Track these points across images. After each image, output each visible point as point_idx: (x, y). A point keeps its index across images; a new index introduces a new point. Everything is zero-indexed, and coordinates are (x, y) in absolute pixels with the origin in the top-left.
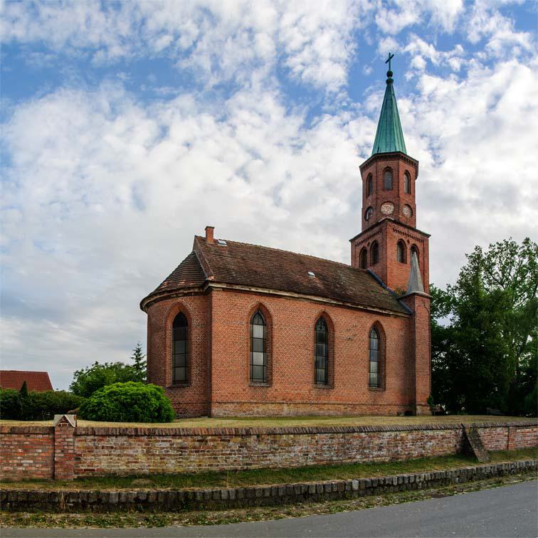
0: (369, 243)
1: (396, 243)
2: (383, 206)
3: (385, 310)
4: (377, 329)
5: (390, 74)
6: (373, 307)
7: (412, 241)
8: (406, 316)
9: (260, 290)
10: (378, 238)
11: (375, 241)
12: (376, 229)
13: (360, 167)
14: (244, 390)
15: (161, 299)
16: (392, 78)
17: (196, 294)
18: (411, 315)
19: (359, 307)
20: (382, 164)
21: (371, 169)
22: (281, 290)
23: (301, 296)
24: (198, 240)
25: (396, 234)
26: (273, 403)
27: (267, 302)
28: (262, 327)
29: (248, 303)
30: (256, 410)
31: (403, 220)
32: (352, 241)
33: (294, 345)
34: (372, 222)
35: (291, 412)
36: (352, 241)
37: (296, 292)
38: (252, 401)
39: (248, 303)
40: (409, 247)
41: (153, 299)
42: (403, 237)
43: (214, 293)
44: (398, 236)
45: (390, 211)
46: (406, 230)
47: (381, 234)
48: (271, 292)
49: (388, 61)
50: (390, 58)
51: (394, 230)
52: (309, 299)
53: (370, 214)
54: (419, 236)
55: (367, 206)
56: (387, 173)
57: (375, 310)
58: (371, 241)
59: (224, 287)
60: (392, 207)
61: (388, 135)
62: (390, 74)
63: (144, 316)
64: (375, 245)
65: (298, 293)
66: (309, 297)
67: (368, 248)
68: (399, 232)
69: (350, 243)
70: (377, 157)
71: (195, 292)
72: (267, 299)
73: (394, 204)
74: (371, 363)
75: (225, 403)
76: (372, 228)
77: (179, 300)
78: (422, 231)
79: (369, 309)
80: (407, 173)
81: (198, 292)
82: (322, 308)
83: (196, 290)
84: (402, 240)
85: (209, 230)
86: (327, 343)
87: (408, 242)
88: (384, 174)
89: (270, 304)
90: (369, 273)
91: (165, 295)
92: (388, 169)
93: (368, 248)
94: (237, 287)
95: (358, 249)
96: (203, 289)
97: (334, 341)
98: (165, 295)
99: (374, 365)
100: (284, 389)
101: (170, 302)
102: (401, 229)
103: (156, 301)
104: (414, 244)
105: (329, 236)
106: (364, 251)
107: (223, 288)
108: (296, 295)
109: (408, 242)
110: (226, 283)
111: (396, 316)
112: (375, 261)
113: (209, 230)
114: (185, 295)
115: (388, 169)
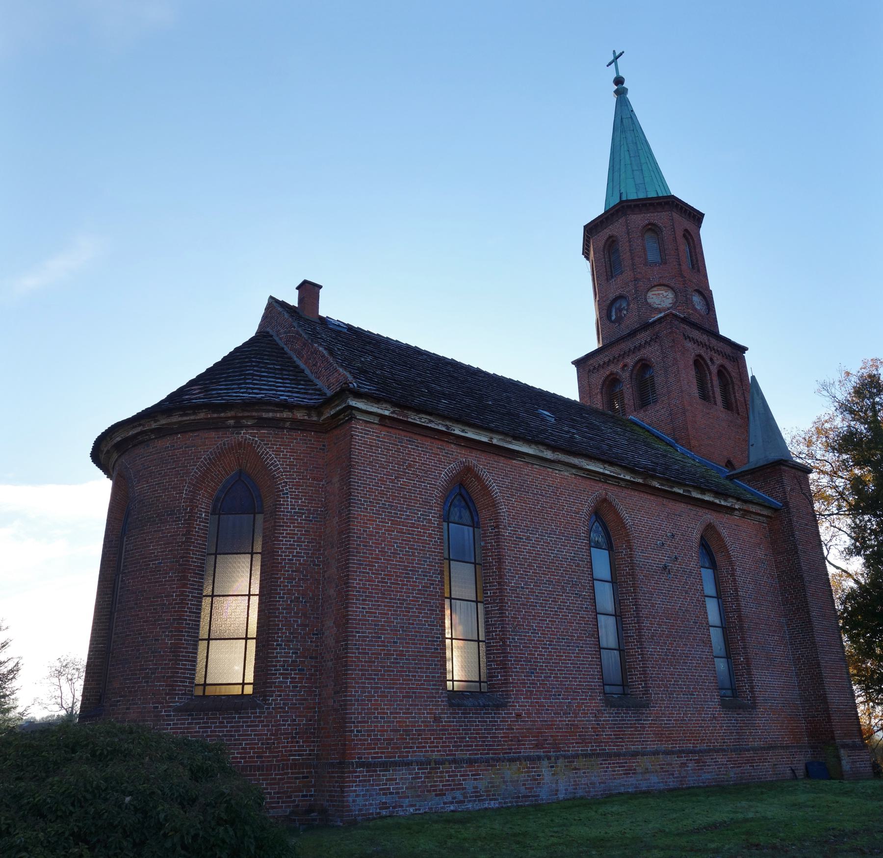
0: (625, 366)
1: (691, 362)
2: (650, 294)
3: (725, 495)
5: (619, 81)
8: (765, 512)
9: (471, 435)
10: (652, 353)
13: (585, 227)
15: (184, 429)
17: (298, 426)
19: (676, 490)
20: (638, 220)
21: (616, 229)
25: (689, 345)
27: (480, 463)
28: (471, 529)
29: (439, 465)
30: (469, 785)
31: (695, 319)
32: (578, 363)
33: (550, 582)
34: (631, 321)
35: (562, 787)
36: (578, 363)
37: (549, 447)
38: (459, 755)
39: (439, 465)
40: (714, 369)
41: (154, 425)
42: (702, 351)
43: (358, 429)
44: (693, 350)
46: (704, 338)
47: (656, 347)
48: (495, 441)
50: (617, 58)
51: (686, 337)
52: (574, 466)
54: (728, 350)
55: (612, 296)
56: (647, 236)
57: (707, 498)
58: (630, 361)
59: (387, 413)
61: (637, 173)
62: (619, 81)
63: (101, 487)
64: (644, 366)
67: (625, 376)
68: (695, 341)
69: (574, 369)
70: (618, 211)
71: (294, 421)
72: (483, 458)
73: (672, 289)
75: (385, 766)
76: (622, 339)
77: (245, 435)
78: (733, 339)
81: (301, 422)
82: (600, 489)
83: (300, 415)
84: (700, 356)
85: (309, 291)
87: (711, 360)
88: (643, 236)
89: (494, 475)
91: (201, 416)
92: (652, 228)
93: (625, 376)
95: (598, 379)
96: (320, 414)
97: (633, 575)
98: (201, 416)
100: (538, 713)
101: (208, 444)
102: (696, 334)
103: (162, 433)
104: (722, 366)
106: (612, 382)
108: (548, 454)
109: (711, 360)
110: (394, 404)
111: (745, 513)
113: (309, 291)
114: (262, 423)
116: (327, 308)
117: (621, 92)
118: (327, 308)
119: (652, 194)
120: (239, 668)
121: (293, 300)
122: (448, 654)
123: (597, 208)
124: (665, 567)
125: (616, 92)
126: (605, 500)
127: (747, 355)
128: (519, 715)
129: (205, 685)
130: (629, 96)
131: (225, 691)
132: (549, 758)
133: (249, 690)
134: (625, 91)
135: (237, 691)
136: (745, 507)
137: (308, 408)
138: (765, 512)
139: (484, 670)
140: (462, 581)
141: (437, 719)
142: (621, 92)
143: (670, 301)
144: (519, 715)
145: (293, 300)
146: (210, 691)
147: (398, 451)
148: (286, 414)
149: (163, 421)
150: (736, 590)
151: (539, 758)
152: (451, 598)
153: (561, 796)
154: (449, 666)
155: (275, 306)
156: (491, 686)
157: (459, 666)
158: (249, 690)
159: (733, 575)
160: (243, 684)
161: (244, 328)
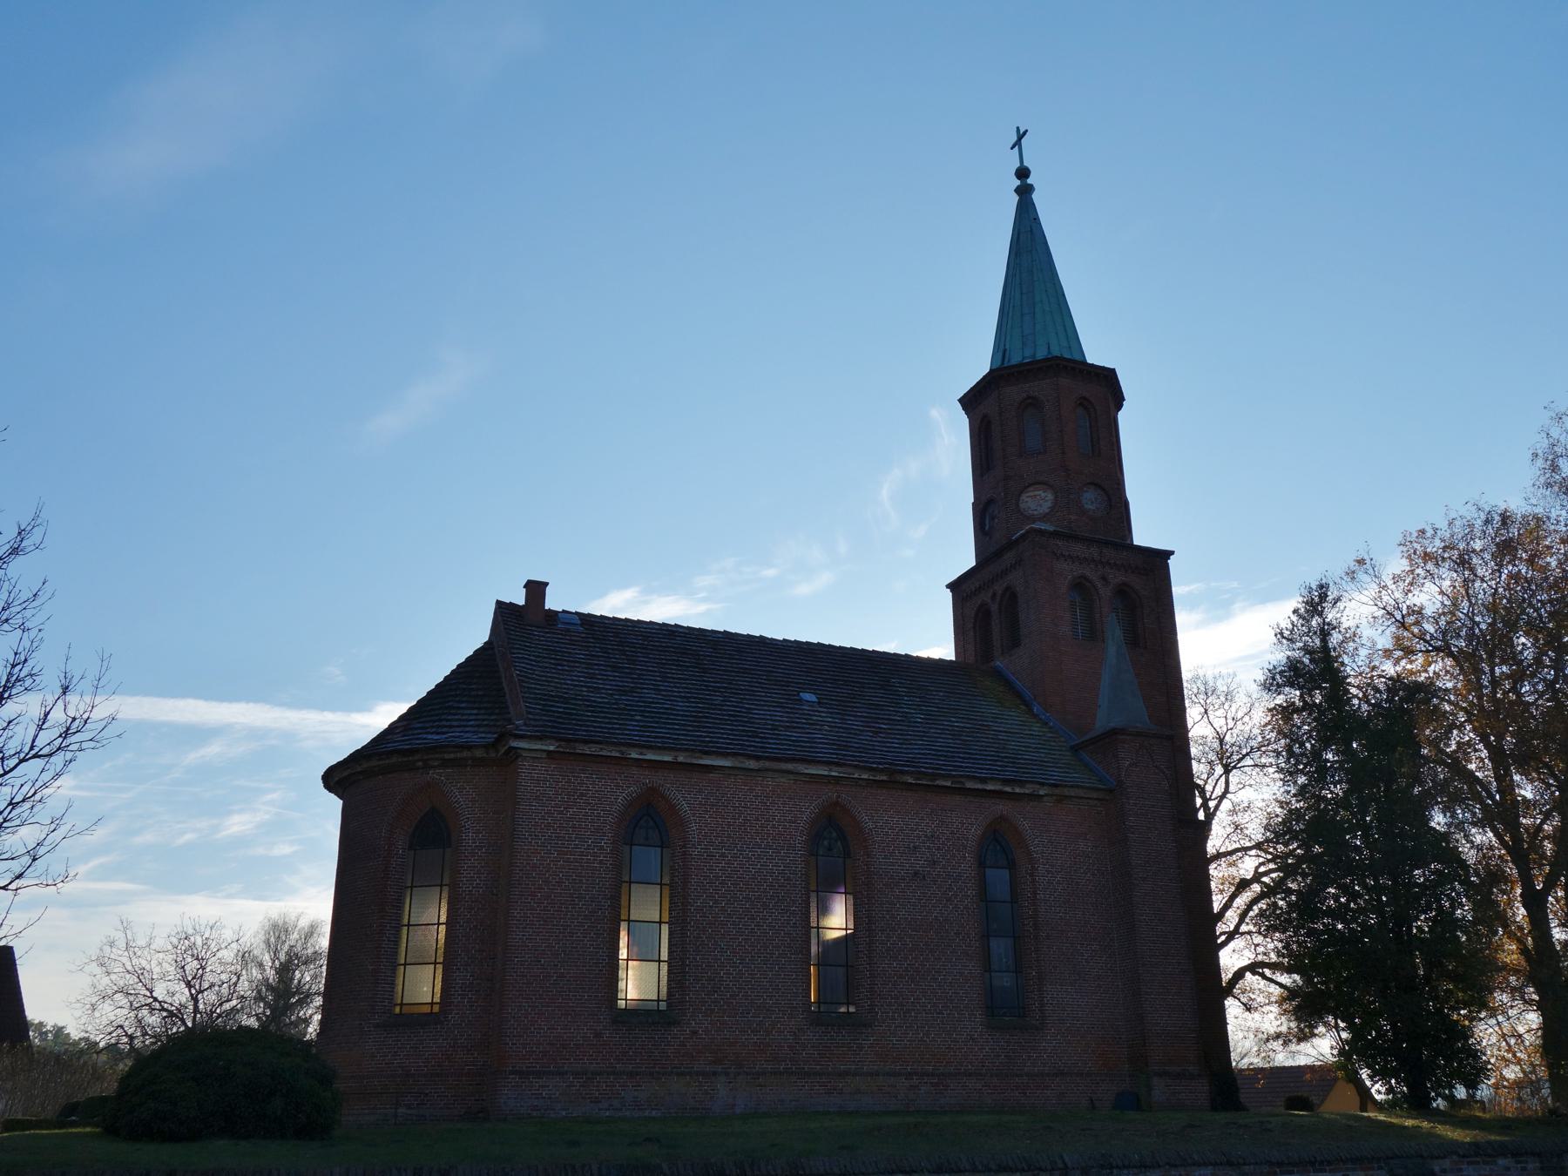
0: (994, 595)
2: (1024, 497)
3: (1022, 783)
4: (999, 845)
5: (1023, 173)
6: (984, 780)
7: (1117, 578)
8: (1095, 795)
11: (1008, 588)
12: (1009, 557)
14: (598, 1035)
16: (1029, 181)
18: (1111, 791)
20: (1014, 393)
22: (707, 753)
23: (767, 764)
24: (504, 611)
26: (683, 1074)
32: (951, 586)
37: (749, 757)
45: (1045, 507)
48: (681, 759)
49: (1018, 143)
53: (993, 518)
57: (990, 787)
58: (999, 588)
60: (1050, 496)
62: (1023, 173)
64: (1011, 597)
65: (758, 758)
66: (790, 766)
67: (994, 608)
69: (948, 594)
73: (1051, 487)
74: (994, 943)
76: (998, 554)
79: (970, 785)
80: (1083, 402)
83: (479, 753)
85: (536, 590)
86: (1012, 866)
87: (1104, 578)
89: (682, 796)
90: (998, 674)
92: (1032, 403)
94: (587, 749)
99: (1001, 948)
104: (1124, 584)
105: (883, 574)
106: (983, 615)
107: (549, 752)
108: (752, 764)
109: (1104, 578)
111: (1061, 799)
112: (1014, 641)
113: (536, 590)
114: (445, 764)
115: (1032, 403)
116: (553, 602)
117: (1025, 192)
118: (554, 601)
119: (1041, 354)
120: (427, 989)
121: (519, 598)
122: (622, 974)
123: (979, 365)
124: (916, 873)
125: (1017, 190)
126: (837, 804)
127: (1172, 562)
128: (695, 1033)
129: (402, 1004)
130: (1035, 196)
131: (416, 1010)
132: (727, 1074)
133: (436, 1009)
134: (1030, 188)
135: (427, 1009)
136: (1057, 791)
137: (486, 747)
138: (1095, 795)
139: (664, 990)
140: (647, 905)
141: (598, 1035)
142: (1025, 192)
143: (1049, 504)
144: (695, 1033)
145: (519, 598)
146: (406, 1010)
147: (569, 781)
148: (465, 754)
149: (365, 765)
150: (1035, 894)
151: (714, 1074)
152: (629, 921)
153: (738, 1111)
154: (622, 985)
155: (503, 610)
156: (669, 1005)
157: (637, 983)
158: (436, 1009)
159: (1032, 875)
160: (432, 1004)
161: (475, 633)
